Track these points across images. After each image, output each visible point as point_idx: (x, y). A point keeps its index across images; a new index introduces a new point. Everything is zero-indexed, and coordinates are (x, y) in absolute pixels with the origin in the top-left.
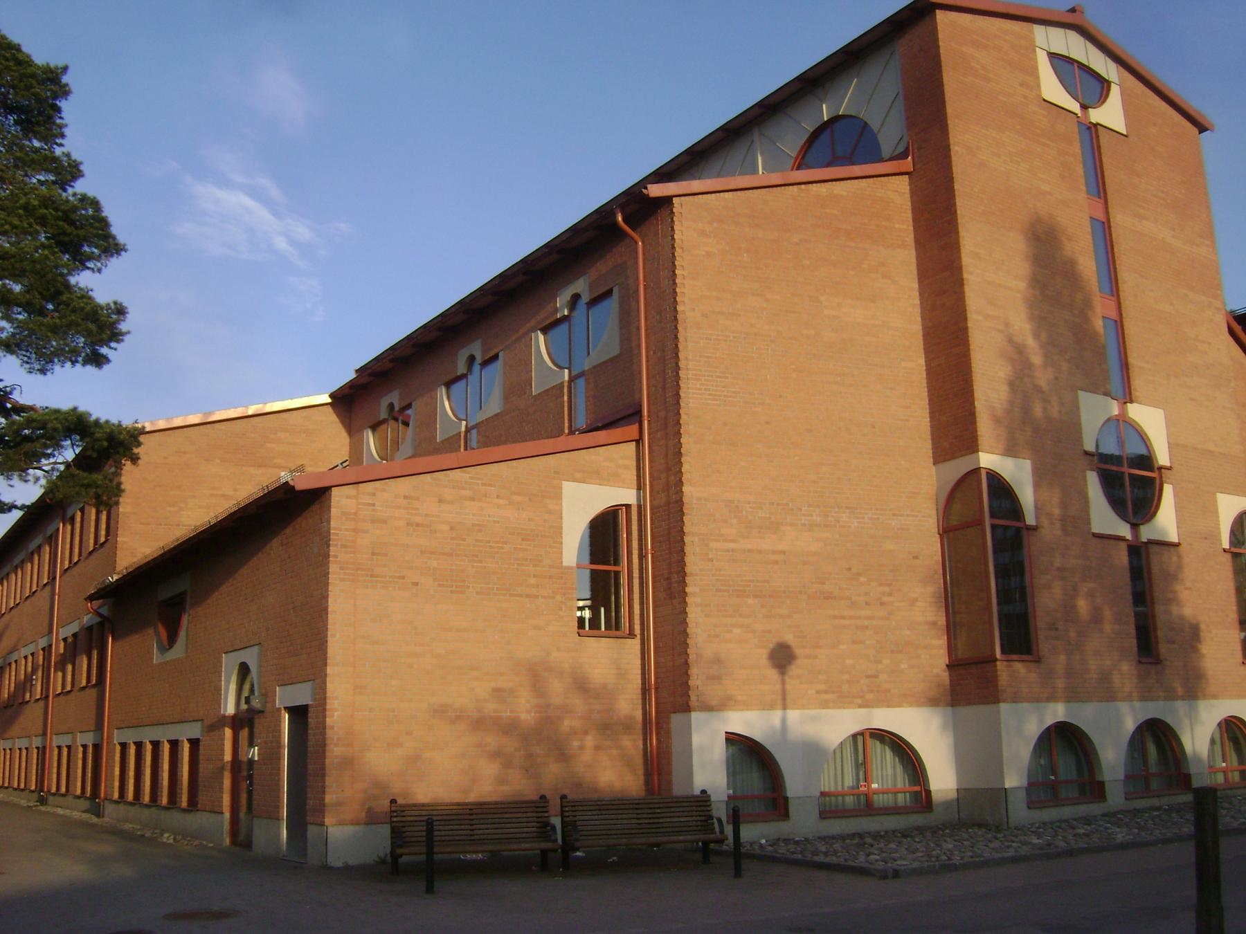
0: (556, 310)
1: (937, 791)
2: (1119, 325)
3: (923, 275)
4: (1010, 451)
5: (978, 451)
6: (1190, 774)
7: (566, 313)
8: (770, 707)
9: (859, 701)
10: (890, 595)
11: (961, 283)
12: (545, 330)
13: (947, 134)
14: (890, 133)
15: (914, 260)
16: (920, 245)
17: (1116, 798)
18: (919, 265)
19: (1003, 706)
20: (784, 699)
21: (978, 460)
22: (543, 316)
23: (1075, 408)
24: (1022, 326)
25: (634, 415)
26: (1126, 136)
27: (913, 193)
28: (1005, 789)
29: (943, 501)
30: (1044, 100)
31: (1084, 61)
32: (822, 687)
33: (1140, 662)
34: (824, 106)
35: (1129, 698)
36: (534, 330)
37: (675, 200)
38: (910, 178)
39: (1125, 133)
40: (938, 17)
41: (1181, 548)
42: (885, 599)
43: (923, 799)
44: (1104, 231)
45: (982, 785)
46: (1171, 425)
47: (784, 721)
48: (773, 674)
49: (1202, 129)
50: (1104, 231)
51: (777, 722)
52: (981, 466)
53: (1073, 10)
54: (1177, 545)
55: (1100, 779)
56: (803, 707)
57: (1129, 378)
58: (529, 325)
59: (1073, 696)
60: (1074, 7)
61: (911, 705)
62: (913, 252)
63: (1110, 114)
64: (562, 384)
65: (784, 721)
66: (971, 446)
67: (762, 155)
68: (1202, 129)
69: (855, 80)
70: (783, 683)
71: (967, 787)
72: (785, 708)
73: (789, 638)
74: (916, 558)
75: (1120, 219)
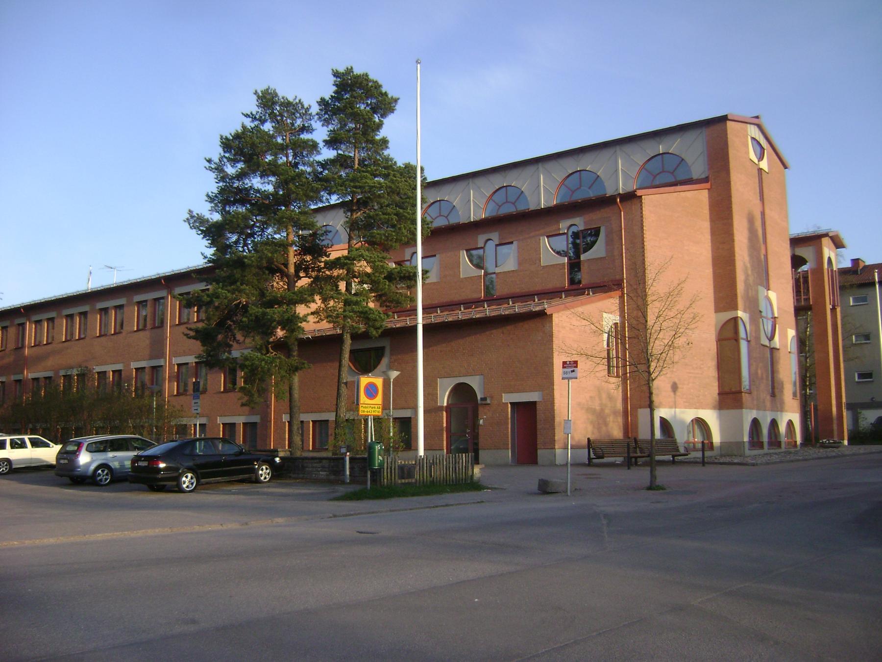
0: (559, 229)
1: (716, 443)
2: (766, 256)
3: (713, 233)
4: (745, 311)
5: (737, 310)
6: (780, 441)
7: (566, 232)
8: (671, 407)
9: (694, 406)
10: (703, 365)
11: (733, 241)
12: (548, 237)
13: (730, 177)
14: (698, 169)
15: (709, 227)
16: (712, 220)
17: (799, 448)
18: (711, 229)
19: (744, 410)
20: (675, 404)
21: (737, 314)
22: (551, 229)
23: (757, 291)
24: (747, 258)
25: (618, 285)
26: (768, 173)
27: (710, 197)
28: (744, 442)
29: (719, 328)
30: (750, 159)
31: (758, 140)
32: (685, 400)
33: (793, 399)
34: (661, 146)
35: (769, 410)
36: (543, 235)
37: (643, 197)
38: (709, 191)
39: (767, 171)
40: (728, 124)
41: (780, 351)
42: (702, 366)
43: (707, 445)
44: (763, 214)
45: (732, 440)
46: (778, 298)
47: (675, 412)
48: (672, 394)
49: (786, 167)
50: (763, 214)
51: (673, 413)
52: (739, 316)
53: (757, 117)
54: (778, 349)
55: (761, 441)
56: (680, 408)
57: (768, 279)
58: (542, 231)
59: (758, 409)
60: (758, 116)
61: (708, 409)
62: (709, 223)
63: (764, 165)
64: (564, 263)
65: (675, 412)
66: (735, 308)
67: (621, 159)
68: (786, 167)
69: (679, 140)
70: (675, 398)
71: (726, 441)
72: (675, 408)
73: (676, 380)
74: (710, 350)
75: (767, 211)
